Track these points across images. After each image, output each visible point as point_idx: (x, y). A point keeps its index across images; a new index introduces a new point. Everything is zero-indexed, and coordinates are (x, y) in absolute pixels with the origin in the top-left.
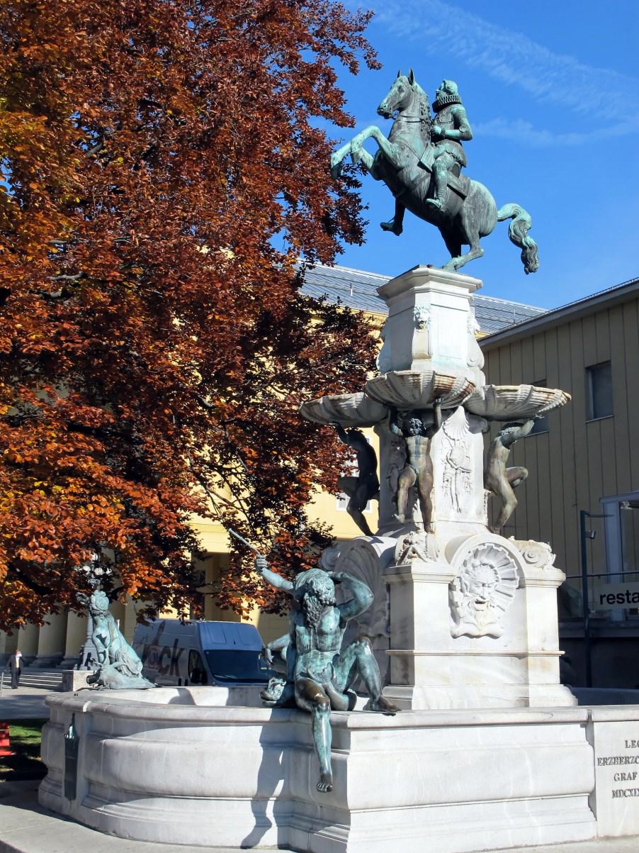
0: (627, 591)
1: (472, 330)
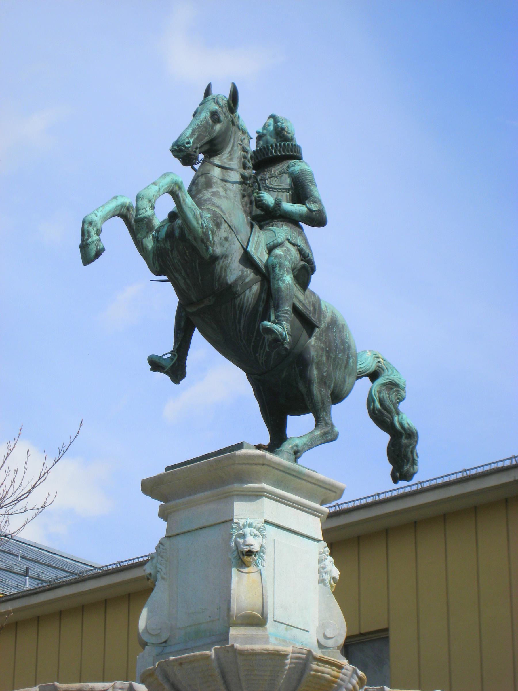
1: (327, 577)
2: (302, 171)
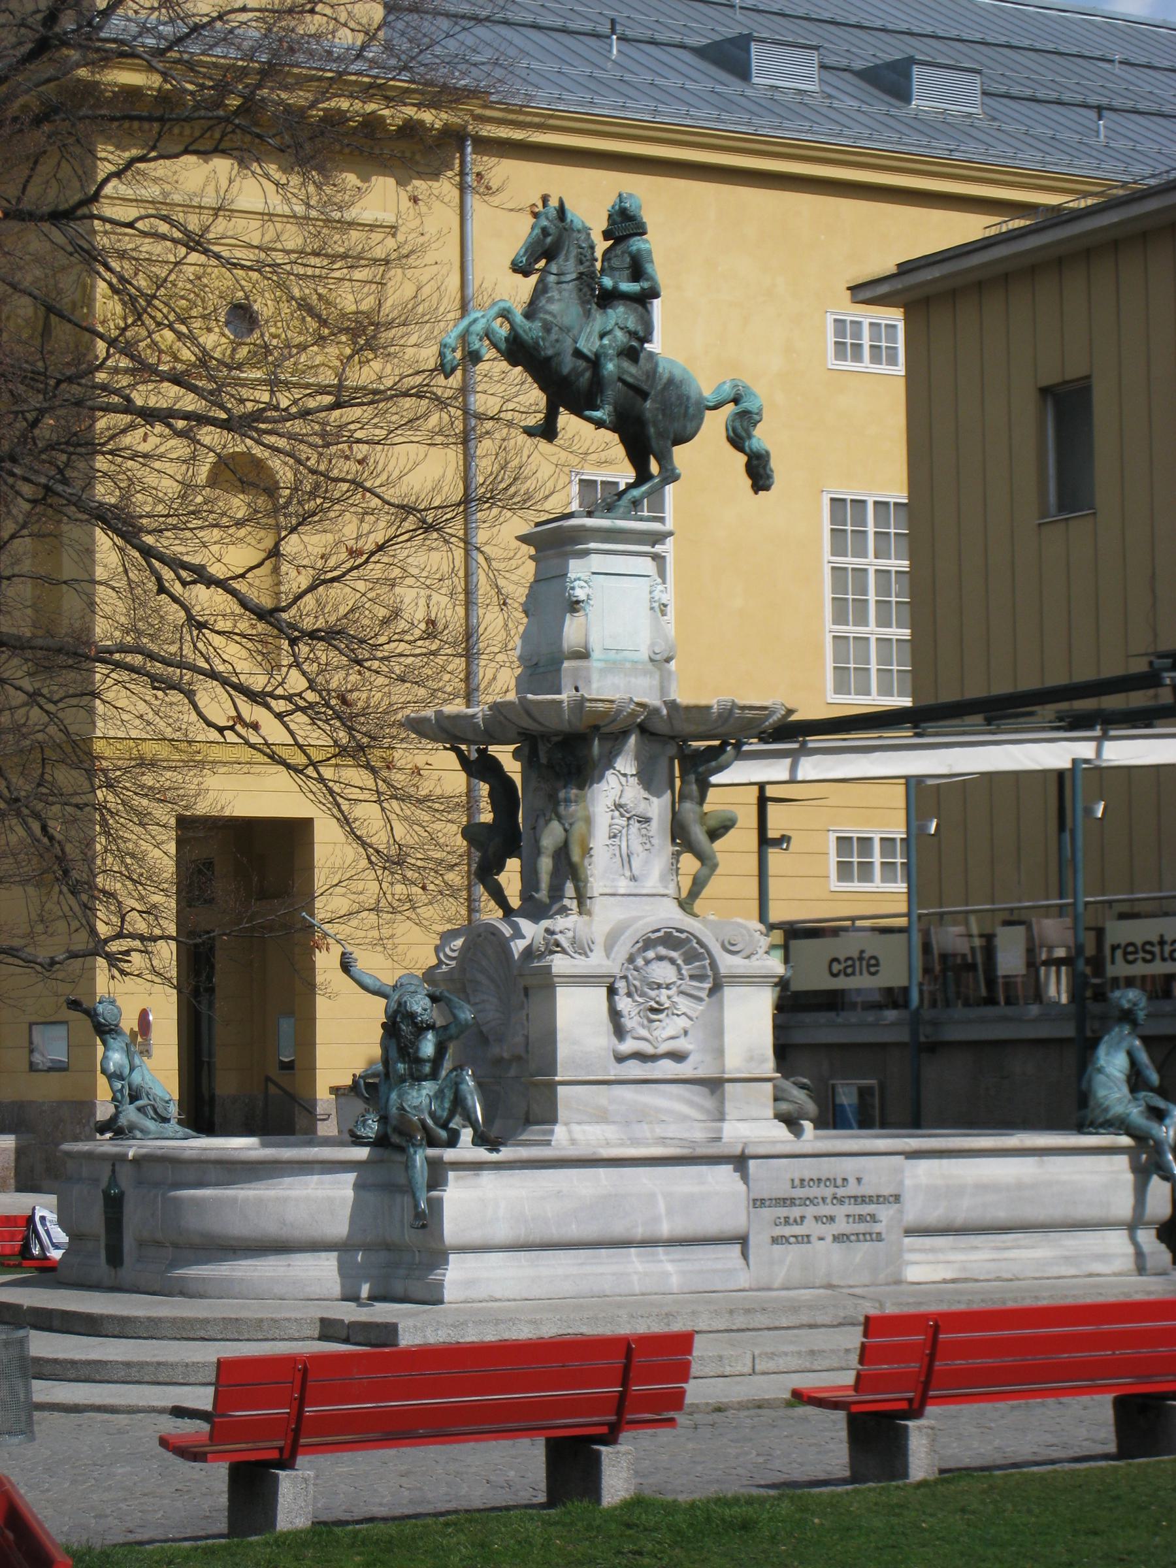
0: (1162, 936)
2: (639, 251)
